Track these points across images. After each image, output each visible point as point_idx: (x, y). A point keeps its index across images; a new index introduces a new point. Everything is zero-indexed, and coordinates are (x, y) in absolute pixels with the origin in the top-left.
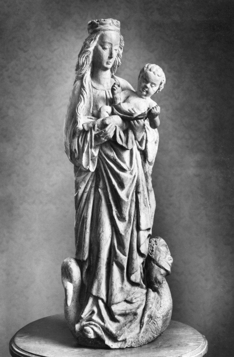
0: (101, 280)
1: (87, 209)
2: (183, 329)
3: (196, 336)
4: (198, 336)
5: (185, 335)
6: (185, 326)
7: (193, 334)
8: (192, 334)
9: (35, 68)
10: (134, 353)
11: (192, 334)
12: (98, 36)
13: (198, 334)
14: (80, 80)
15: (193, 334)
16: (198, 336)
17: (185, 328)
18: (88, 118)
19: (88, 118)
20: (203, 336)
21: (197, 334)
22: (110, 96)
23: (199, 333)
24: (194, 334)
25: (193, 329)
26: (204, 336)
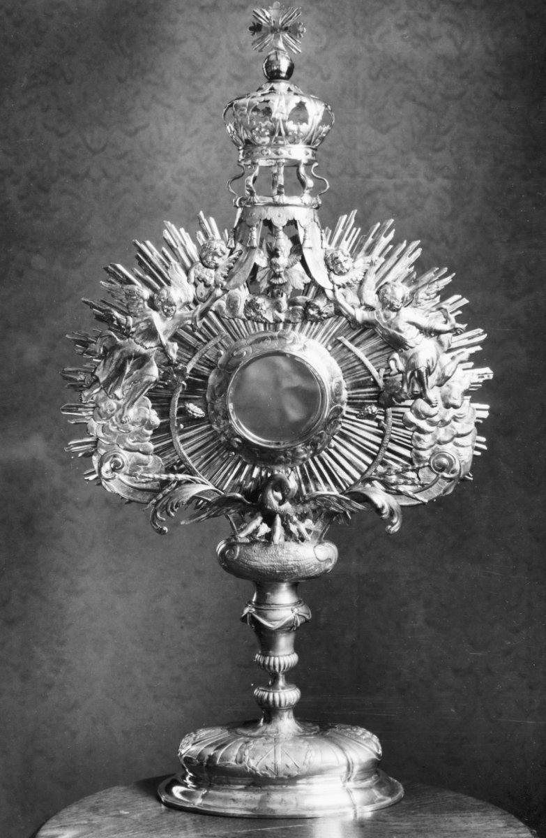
0: (70, 492)
1: (234, 470)
2: (477, 814)
3: (514, 830)
4: (519, 831)
5: (486, 829)
6: (482, 805)
7: (505, 827)
8: (501, 825)
9: (87, 174)
10: (445, 456)
11: (501, 825)
12: (349, 499)
13: (519, 827)
14: (267, 602)
15: (505, 827)
16: (519, 831)
17: (483, 810)
18: (464, 369)
19: (464, 369)
20: (531, 832)
21: (515, 825)
22: (166, 360)
23: (521, 824)
24: (509, 825)
25: (505, 814)
26: (535, 831)
